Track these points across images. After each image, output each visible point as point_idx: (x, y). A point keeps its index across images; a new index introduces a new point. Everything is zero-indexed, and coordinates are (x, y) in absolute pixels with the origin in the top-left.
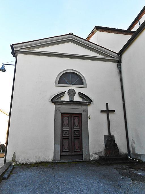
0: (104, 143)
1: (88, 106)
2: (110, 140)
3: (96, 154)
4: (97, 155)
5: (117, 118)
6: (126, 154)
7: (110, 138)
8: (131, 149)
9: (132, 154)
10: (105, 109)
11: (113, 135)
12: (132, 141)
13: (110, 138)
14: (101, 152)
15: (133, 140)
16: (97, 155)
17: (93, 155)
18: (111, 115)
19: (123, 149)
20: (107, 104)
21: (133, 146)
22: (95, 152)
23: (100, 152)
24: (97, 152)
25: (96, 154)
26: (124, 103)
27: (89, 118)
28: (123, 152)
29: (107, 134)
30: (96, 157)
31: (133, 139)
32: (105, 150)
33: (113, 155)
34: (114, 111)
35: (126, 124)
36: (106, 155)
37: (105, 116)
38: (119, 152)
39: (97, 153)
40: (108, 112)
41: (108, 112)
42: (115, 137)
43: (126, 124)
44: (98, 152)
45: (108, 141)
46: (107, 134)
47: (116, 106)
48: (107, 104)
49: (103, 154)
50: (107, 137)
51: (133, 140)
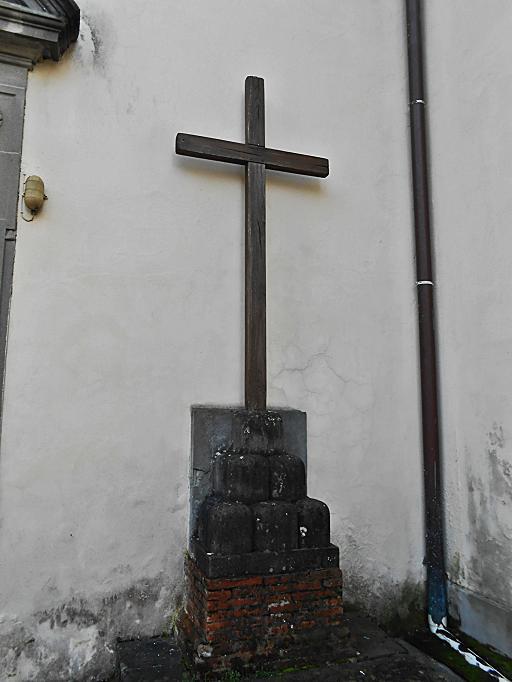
0: (185, 495)
1: (35, 79)
2: (253, 473)
3: (72, 614)
4: (92, 631)
5: (339, 249)
6: (408, 589)
7: (258, 443)
8: (460, 546)
9: (471, 598)
10: (233, 132)
11: (295, 406)
12: (484, 473)
13: (258, 443)
14: (140, 596)
15: (492, 456)
16: (92, 631)
17: (46, 633)
18: (279, 201)
19: (378, 548)
20: (255, 86)
21: (493, 530)
22: (64, 596)
23: (131, 593)
24: (96, 588)
25: (76, 615)
26: (423, 109)
27: (35, 209)
28: (383, 570)
29: (231, 395)
30: (73, 651)
31: (501, 455)
32: (197, 565)
33: (260, 650)
34: (319, 167)
35: (426, 302)
36: (190, 630)
37: (226, 197)
38: (347, 576)
39: (95, 611)
40: (253, 163)
41: (253, 163)
42: (422, 559)
43: (426, 302)
44: (105, 589)
45: (227, 471)
46: (231, 395)
47: (336, 110)
48: (255, 86)
49: (169, 613)
50: (226, 426)
51: (492, 456)
